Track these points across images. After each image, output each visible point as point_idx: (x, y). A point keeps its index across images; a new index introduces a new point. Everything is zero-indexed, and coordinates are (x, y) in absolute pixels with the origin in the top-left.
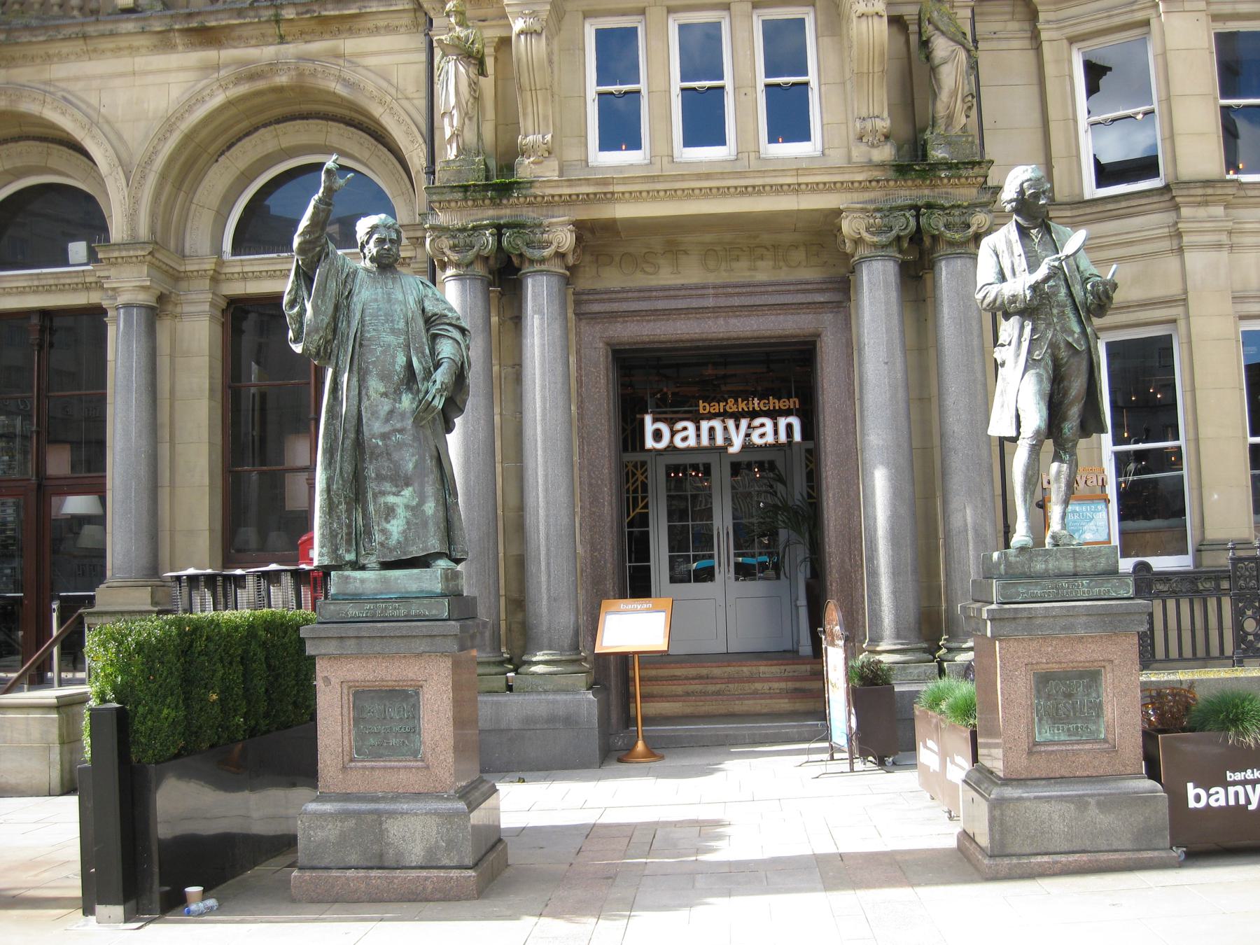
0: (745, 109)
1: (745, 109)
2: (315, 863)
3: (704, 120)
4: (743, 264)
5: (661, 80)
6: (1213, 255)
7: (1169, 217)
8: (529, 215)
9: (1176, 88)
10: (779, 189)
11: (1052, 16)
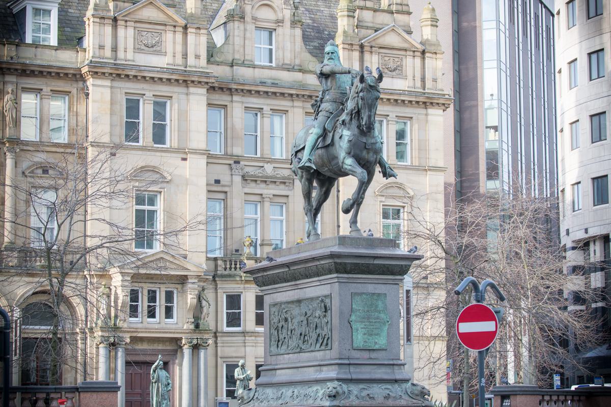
0: (160, 311)
1: (160, 311)
2: (319, 368)
3: (152, 314)
4: (156, 345)
5: (143, 304)
6: (251, 348)
7: (244, 338)
8: (121, 335)
9: (247, 310)
10: (170, 333)
11: (220, 286)
